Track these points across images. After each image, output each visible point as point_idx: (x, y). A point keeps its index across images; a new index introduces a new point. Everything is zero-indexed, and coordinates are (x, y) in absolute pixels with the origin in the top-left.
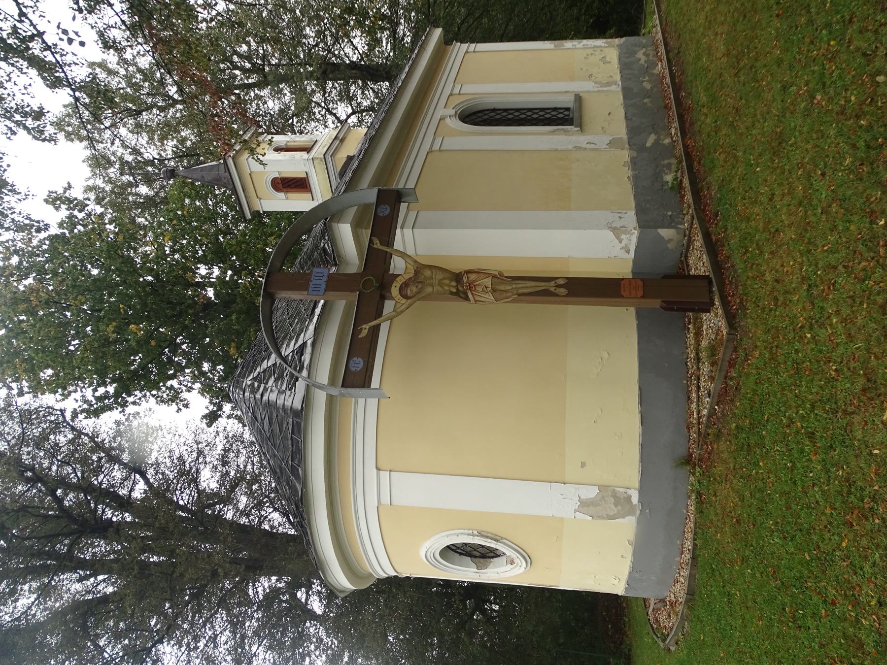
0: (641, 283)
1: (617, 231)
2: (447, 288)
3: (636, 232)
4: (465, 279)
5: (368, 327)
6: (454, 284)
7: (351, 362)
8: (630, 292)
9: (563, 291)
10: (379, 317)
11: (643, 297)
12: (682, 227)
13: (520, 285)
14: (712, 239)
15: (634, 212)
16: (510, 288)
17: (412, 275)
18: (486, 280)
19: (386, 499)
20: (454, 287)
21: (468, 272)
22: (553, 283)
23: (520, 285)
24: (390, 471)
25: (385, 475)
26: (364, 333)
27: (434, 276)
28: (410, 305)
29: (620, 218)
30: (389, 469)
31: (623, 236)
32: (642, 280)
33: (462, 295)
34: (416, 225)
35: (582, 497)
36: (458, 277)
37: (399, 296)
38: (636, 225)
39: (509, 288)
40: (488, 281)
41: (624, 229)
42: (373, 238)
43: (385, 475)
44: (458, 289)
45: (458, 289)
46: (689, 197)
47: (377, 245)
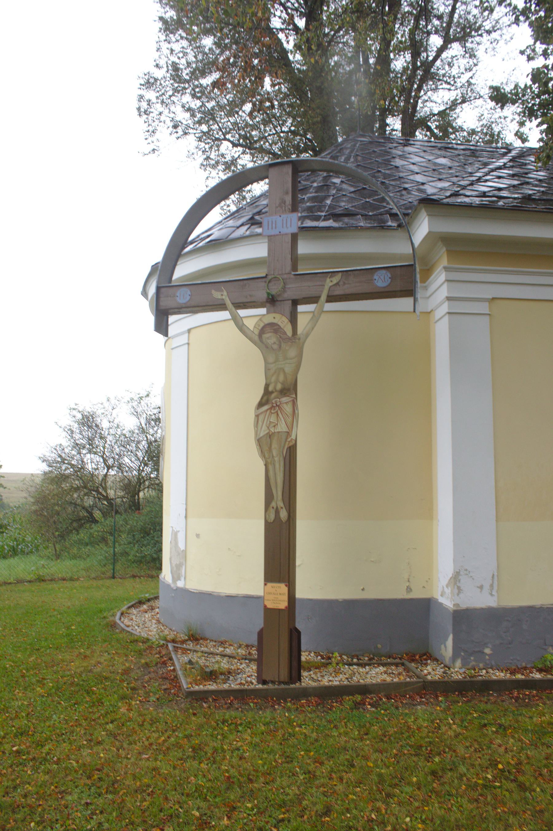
1: (456, 578)
2: (273, 379)
4: (284, 399)
5: (224, 297)
6: (279, 387)
7: (384, 271)
8: (270, 593)
12: (458, 663)
16: (275, 454)
20: (275, 388)
23: (277, 465)
24: (188, 344)
26: (217, 295)
28: (251, 339)
30: (190, 342)
33: (265, 398)
38: (464, 606)
39: (275, 453)
40: (282, 427)
41: (456, 591)
42: (340, 274)
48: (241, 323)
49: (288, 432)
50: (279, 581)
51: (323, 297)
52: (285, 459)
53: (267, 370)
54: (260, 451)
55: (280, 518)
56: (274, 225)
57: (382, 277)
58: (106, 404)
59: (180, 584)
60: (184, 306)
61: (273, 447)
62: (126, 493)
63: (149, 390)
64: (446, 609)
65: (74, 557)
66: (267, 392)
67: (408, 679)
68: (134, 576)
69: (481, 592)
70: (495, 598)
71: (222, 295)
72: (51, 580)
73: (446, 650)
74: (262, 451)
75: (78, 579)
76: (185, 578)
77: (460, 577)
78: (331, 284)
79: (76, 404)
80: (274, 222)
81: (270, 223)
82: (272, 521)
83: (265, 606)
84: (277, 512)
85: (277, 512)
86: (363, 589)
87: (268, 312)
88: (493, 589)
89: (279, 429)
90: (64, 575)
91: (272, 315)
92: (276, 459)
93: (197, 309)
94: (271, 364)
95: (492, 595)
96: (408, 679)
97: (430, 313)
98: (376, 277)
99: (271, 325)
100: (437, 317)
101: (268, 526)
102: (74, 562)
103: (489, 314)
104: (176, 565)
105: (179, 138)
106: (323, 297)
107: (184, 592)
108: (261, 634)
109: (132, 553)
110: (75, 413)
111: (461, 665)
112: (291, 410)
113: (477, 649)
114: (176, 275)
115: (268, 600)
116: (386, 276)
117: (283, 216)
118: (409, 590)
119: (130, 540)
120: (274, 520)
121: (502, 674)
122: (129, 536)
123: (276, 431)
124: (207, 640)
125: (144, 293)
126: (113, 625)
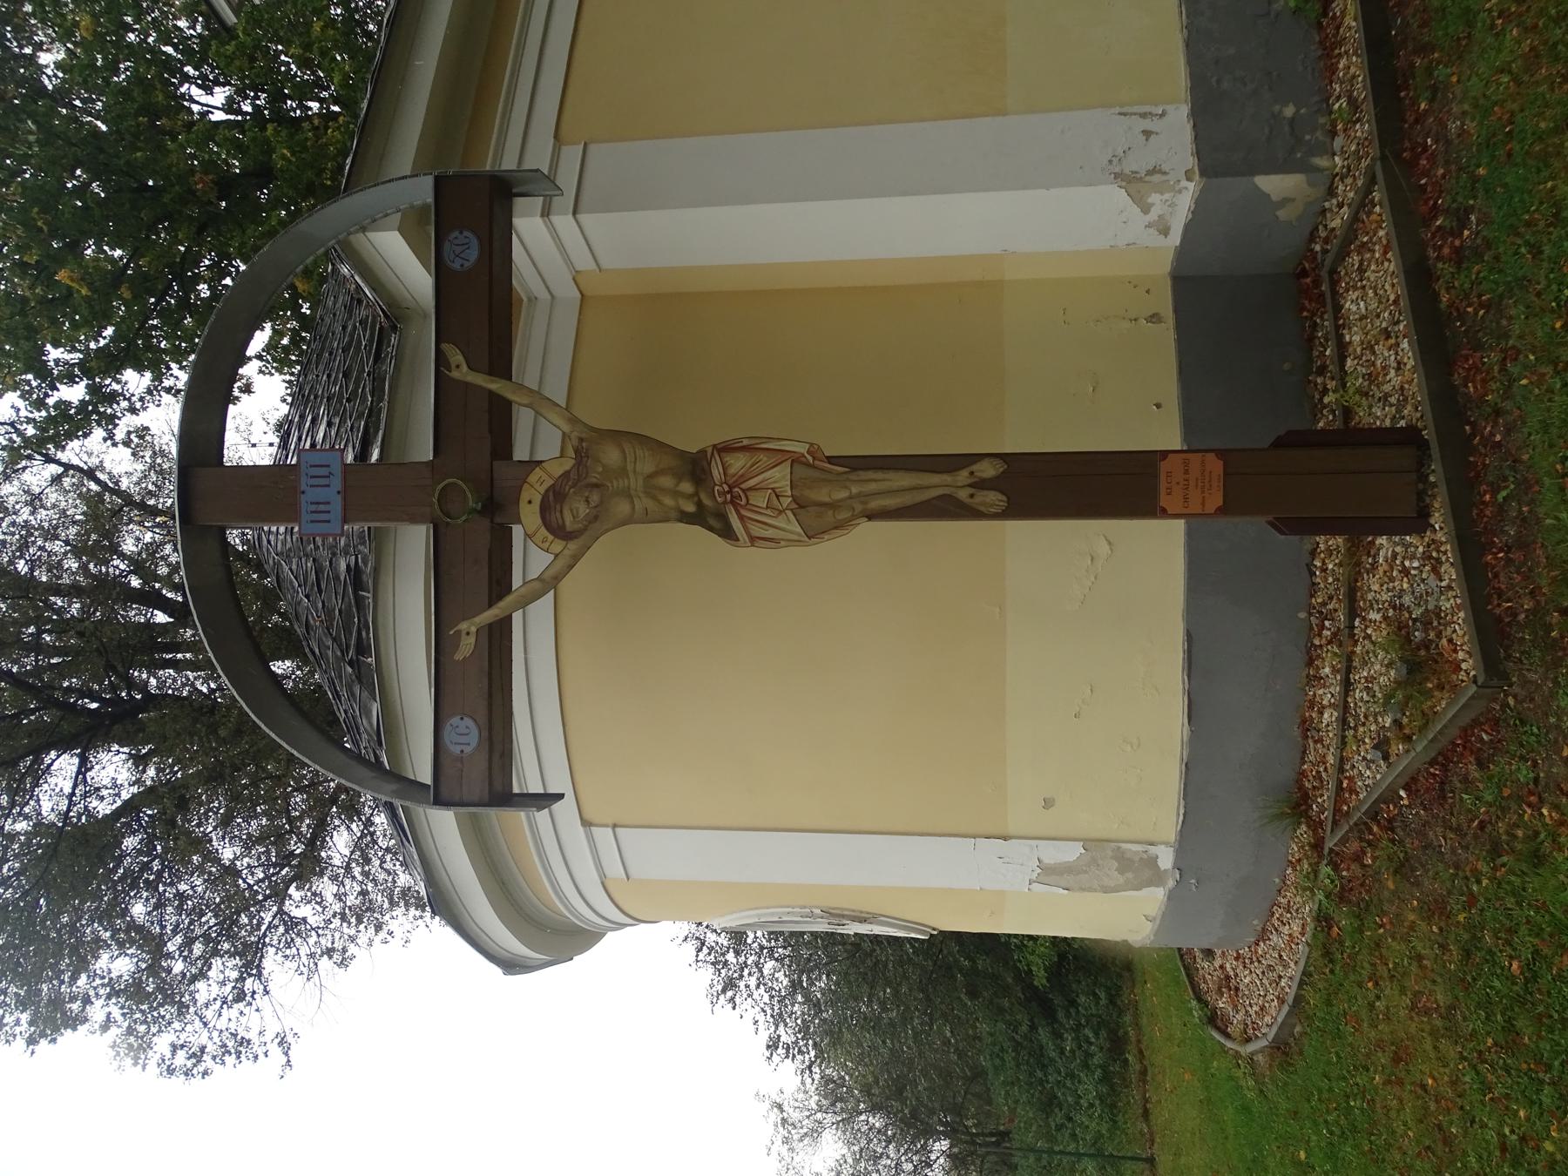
0: (1215, 466)
1: (1135, 183)
2: (668, 501)
3: (1191, 186)
4: (717, 472)
5: (473, 629)
6: (687, 487)
7: (447, 246)
8: (1186, 499)
9: (994, 499)
10: (500, 597)
11: (1222, 511)
12: (1322, 162)
13: (873, 487)
14: (1436, 297)
15: (1185, 110)
16: (843, 494)
18: (776, 473)
19: (614, 869)
20: (689, 497)
21: (724, 449)
22: (963, 476)
23: (873, 487)
24: (615, 826)
25: (603, 835)
26: (467, 646)
27: (630, 467)
28: (576, 559)
29: (1147, 134)
30: (610, 822)
31: (1154, 198)
32: (1221, 453)
33: (712, 522)
34: (585, 198)
35: (1046, 861)
36: (696, 467)
37: (543, 531)
38: (1191, 162)
39: (842, 494)
40: (780, 476)
41: (1156, 178)
42: (444, 346)
43: (603, 835)
44: (699, 504)
45: (699, 504)
46: (1353, 66)
47: (462, 372)
48: (537, 585)
49: (793, 461)
51: (496, 385)
52: (854, 469)
53: (647, 518)
54: (839, 532)
55: (997, 478)
56: (322, 507)
57: (458, 250)
59: (1166, 859)
60: (485, 734)
61: (827, 499)
62: (973, 1163)
63: (767, 1105)
68: (1146, 1114)
69: (1157, 134)
71: (468, 634)
73: (1293, 200)
74: (836, 528)
77: (1127, 171)
78: (465, 368)
80: (314, 508)
82: (1004, 498)
83: (1222, 511)
84: (981, 485)
85: (981, 485)
86: (1158, 406)
87: (519, 521)
88: (1150, 113)
89: (784, 485)
92: (854, 490)
94: (633, 508)
95: (1163, 115)
97: (582, 295)
98: (456, 266)
99: (545, 509)
100: (593, 266)
103: (585, 144)
104: (1121, 871)
105: (265, 990)
106: (496, 385)
107: (1185, 844)
111: (1325, 157)
112: (740, 455)
113: (1287, 129)
115: (1203, 504)
116: (457, 242)
118: (1155, 318)
119: (1067, 1135)
120: (1002, 493)
122: (1060, 1138)
123: (789, 493)
124: (1303, 774)
125: (511, 965)
126: (1281, 1048)
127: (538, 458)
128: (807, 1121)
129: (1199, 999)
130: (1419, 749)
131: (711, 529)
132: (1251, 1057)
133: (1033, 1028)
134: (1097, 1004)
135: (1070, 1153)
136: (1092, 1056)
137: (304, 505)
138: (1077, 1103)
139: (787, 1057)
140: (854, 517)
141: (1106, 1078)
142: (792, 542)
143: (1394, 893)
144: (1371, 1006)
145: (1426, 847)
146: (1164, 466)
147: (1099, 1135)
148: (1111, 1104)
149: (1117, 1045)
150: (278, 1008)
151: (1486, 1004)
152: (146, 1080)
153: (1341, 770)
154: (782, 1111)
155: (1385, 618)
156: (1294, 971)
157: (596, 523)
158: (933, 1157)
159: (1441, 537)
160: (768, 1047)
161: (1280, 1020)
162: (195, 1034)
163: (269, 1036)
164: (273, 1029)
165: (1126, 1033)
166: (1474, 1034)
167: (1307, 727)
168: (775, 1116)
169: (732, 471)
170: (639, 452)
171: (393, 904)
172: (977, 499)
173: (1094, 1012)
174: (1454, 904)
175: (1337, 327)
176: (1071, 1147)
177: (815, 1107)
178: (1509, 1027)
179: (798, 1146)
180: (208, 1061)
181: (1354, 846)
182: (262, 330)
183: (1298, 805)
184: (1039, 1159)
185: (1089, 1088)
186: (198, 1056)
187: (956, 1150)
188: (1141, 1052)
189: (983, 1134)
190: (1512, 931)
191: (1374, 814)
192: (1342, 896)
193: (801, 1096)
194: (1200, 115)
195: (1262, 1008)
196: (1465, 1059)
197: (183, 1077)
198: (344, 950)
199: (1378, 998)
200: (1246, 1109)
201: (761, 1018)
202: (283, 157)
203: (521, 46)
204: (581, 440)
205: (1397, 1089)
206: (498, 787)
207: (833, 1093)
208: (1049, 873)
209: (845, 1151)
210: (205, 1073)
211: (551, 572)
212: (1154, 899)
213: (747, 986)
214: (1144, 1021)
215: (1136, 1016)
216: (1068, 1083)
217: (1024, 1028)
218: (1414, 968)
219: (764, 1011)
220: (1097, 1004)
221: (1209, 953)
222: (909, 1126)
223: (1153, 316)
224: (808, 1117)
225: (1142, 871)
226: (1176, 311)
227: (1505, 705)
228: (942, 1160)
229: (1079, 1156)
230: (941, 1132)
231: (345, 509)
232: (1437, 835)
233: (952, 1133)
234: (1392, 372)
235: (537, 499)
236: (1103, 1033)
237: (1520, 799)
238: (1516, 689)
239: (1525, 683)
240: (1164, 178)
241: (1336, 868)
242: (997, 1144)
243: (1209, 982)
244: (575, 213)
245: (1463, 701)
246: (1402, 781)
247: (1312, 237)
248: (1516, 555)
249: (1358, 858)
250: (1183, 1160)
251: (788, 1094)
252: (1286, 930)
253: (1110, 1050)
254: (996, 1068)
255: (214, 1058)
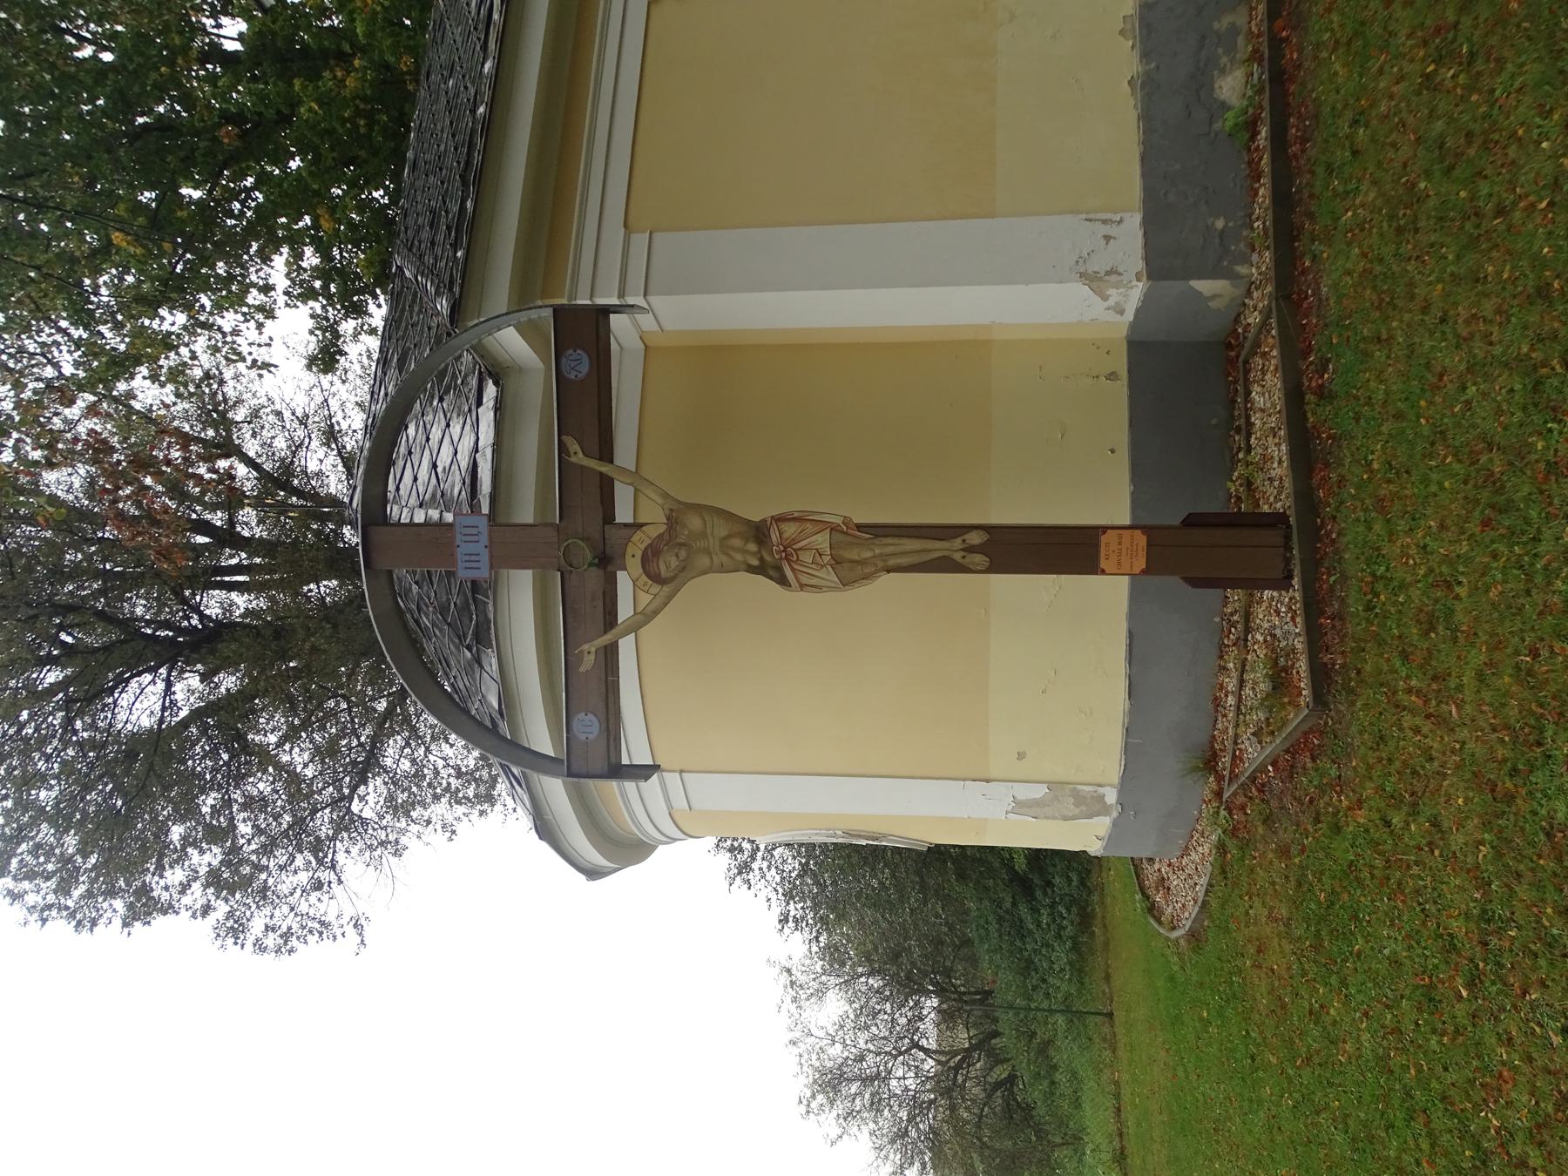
0: (1141, 539)
1: (1092, 279)
2: (739, 557)
4: (774, 537)
5: (593, 649)
6: (752, 547)
7: (564, 360)
8: (1119, 563)
9: (979, 559)
12: (1242, 269)
15: (1138, 217)
17: (663, 528)
19: (680, 803)
20: (754, 554)
21: (780, 519)
23: (890, 549)
24: (681, 772)
26: (589, 662)
27: (709, 531)
28: (670, 598)
29: (1107, 238)
30: (678, 769)
31: (1111, 291)
33: (771, 572)
35: (1019, 797)
36: (759, 532)
37: (644, 578)
38: (1140, 265)
40: (822, 540)
41: (1114, 278)
42: (564, 438)
44: (762, 559)
45: (762, 559)
47: (579, 458)
50: (1097, 546)
51: (604, 468)
52: (877, 536)
53: (723, 569)
56: (473, 558)
57: (573, 364)
58: (802, 1047)
59: (1111, 797)
60: (604, 725)
61: (857, 558)
62: (961, 1017)
63: (777, 970)
64: (1147, 298)
65: (1077, 1104)
66: (761, 570)
67: (1273, 332)
68: (1107, 978)
70: (1126, 216)
72: (1121, 1135)
73: (1220, 296)
75: (1117, 1084)
76: (1100, 786)
77: (1090, 271)
78: (581, 455)
79: (801, 1102)
80: (467, 558)
81: (468, 565)
83: (1143, 572)
84: (971, 549)
85: (971, 549)
86: (1112, 451)
90: (1110, 1113)
91: (630, 561)
92: (877, 551)
93: (612, 721)
96: (1273, 332)
98: (572, 376)
100: (655, 328)
101: (994, 568)
102: (1087, 1106)
104: (1077, 805)
106: (604, 468)
107: (1127, 784)
108: (1196, 582)
109: (1064, 987)
110: (814, 1105)
112: (792, 524)
113: (1217, 240)
114: (549, 751)
117: (458, 543)
118: (1112, 376)
121: (1261, 192)
124: (1214, 736)
125: (593, 873)
126: (1194, 936)
127: (641, 520)
128: (812, 983)
129: (1143, 893)
130: (1278, 742)
131: (771, 578)
132: (1177, 939)
133: (1014, 904)
134: (1070, 885)
135: (1044, 1010)
136: (1064, 928)
137: (459, 556)
138: (1051, 968)
139: (797, 929)
140: (877, 571)
141: (1076, 947)
142: (831, 589)
143: (1263, 836)
144: (1247, 913)
145: (1281, 808)
146: (1104, 539)
147: (1067, 996)
148: (1079, 970)
149: (1085, 920)
150: (353, 896)
151: (1307, 920)
152: (239, 957)
153: (1236, 743)
154: (791, 975)
155: (1265, 641)
156: (1204, 881)
157: (684, 573)
158: (925, 1012)
159: (1297, 595)
160: (780, 921)
161: (1193, 916)
162: (283, 917)
163: (346, 919)
164: (349, 912)
165: (1093, 910)
166: (1300, 938)
167: (1217, 703)
168: (785, 979)
169: (786, 535)
170: (715, 520)
171: (436, 798)
172: (967, 560)
173: (1067, 891)
174: (1294, 850)
175: (1247, 409)
176: (1045, 1005)
177: (820, 970)
178: (1318, 934)
179: (805, 1004)
180: (294, 942)
181: (1241, 799)
182: (281, 254)
183: (1209, 762)
184: (1017, 1014)
185: (1061, 955)
186: (287, 936)
187: (945, 1006)
188: (1105, 926)
189: (969, 993)
190: (1322, 873)
191: (1253, 778)
192: (1233, 833)
193: (808, 962)
194: (1151, 224)
195: (1184, 905)
196: (1295, 954)
197: (273, 954)
198: (397, 842)
199: (1251, 907)
200: (1172, 979)
201: (773, 896)
202: (310, 110)
203: (591, 141)
204: (671, 510)
205: (1258, 971)
206: (613, 760)
207: (834, 956)
208: (1020, 806)
209: (847, 1007)
210: (291, 951)
211: (650, 609)
212: (1103, 825)
213: (761, 869)
214: (1109, 900)
215: (1102, 895)
216: (1044, 951)
217: (1008, 905)
218: (1270, 891)
219: (776, 890)
220: (1070, 885)
221: (1151, 860)
222: (905, 986)
223: (1113, 373)
224: (814, 980)
225: (1091, 806)
226: (1129, 372)
227: (1326, 723)
228: (933, 1015)
229: (1051, 1011)
230: (932, 992)
231: (491, 557)
232: (1288, 802)
233: (941, 992)
234: (1275, 465)
235: (639, 554)
236: (1074, 909)
237: (1332, 787)
238: (1332, 713)
239: (1338, 711)
240: (1120, 278)
241: (1230, 813)
242: (982, 1002)
243: (1150, 881)
244: (645, 295)
245: (1301, 717)
246: (1269, 760)
247: (1237, 320)
248: (1338, 623)
249: (1243, 808)
250: (1132, 1015)
251: (795, 960)
252: (1200, 849)
253: (1079, 924)
254: (981, 939)
255: (298, 938)
